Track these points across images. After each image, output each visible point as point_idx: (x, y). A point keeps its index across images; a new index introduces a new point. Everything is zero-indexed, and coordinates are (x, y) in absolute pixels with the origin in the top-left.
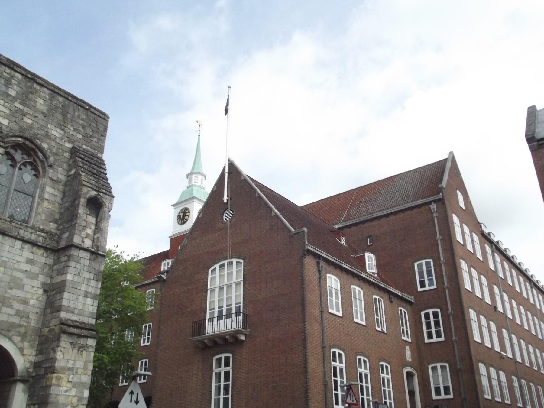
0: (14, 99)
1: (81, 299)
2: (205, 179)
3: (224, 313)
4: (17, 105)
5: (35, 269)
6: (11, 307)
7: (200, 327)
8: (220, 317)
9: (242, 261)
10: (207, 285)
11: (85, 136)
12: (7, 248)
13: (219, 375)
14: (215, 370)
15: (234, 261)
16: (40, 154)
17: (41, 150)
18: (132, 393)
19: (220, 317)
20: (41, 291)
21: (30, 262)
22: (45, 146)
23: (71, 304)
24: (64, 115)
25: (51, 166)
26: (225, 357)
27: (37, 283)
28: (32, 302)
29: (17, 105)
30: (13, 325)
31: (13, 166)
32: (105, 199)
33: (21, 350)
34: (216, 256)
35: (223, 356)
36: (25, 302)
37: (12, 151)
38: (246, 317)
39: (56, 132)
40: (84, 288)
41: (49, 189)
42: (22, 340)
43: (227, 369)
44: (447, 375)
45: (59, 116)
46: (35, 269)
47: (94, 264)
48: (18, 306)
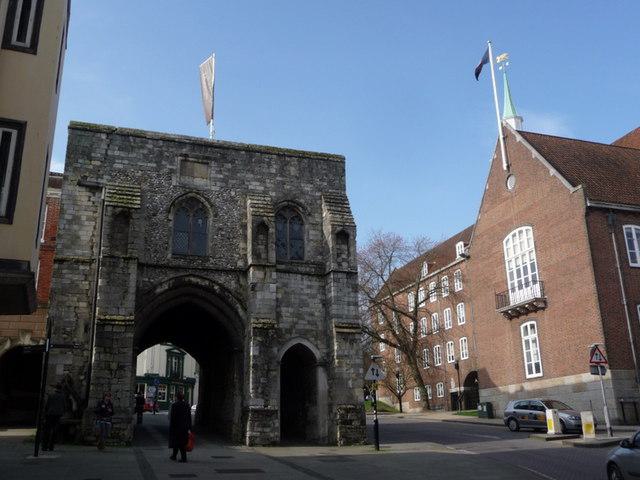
0: (276, 175)
1: (346, 307)
2: (522, 121)
3: (530, 279)
4: (279, 178)
5: (314, 291)
6: (303, 319)
7: (502, 298)
8: (520, 287)
9: (530, 228)
10: (504, 257)
11: (329, 182)
12: (293, 281)
13: (527, 342)
14: (524, 338)
15: (524, 228)
16: (301, 209)
17: (300, 205)
18: (373, 369)
19: (520, 287)
20: (321, 305)
21: (309, 287)
22: (302, 201)
23: (340, 312)
24: (310, 172)
25: (309, 215)
26: (195, 379)
27: (317, 301)
28: (316, 314)
29: (279, 178)
30: (307, 331)
31: (285, 222)
32: (350, 232)
33: (317, 346)
34: (506, 227)
35: (528, 324)
36: (312, 315)
37: (282, 212)
38: (542, 282)
39: (308, 188)
40: (346, 299)
41: (311, 232)
42: (316, 339)
43: (526, 338)
44: (627, 330)
45: (308, 174)
46: (314, 291)
47: (350, 281)
48: (307, 318)
